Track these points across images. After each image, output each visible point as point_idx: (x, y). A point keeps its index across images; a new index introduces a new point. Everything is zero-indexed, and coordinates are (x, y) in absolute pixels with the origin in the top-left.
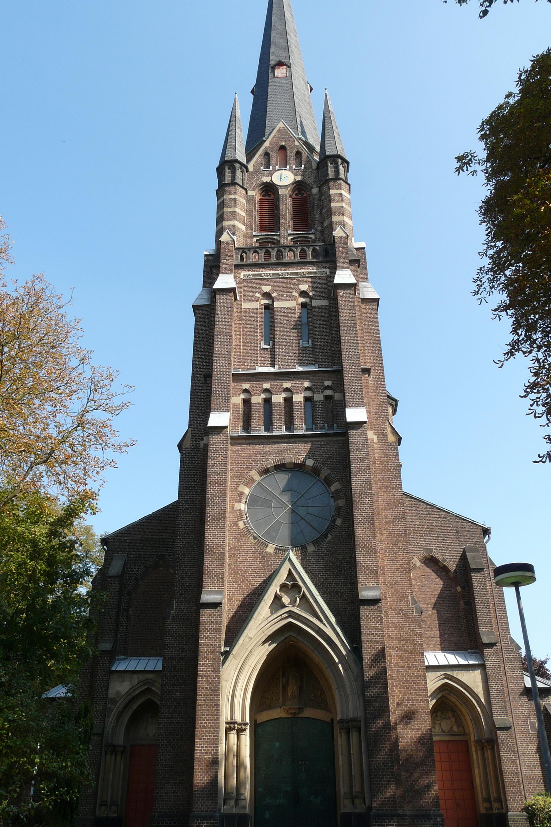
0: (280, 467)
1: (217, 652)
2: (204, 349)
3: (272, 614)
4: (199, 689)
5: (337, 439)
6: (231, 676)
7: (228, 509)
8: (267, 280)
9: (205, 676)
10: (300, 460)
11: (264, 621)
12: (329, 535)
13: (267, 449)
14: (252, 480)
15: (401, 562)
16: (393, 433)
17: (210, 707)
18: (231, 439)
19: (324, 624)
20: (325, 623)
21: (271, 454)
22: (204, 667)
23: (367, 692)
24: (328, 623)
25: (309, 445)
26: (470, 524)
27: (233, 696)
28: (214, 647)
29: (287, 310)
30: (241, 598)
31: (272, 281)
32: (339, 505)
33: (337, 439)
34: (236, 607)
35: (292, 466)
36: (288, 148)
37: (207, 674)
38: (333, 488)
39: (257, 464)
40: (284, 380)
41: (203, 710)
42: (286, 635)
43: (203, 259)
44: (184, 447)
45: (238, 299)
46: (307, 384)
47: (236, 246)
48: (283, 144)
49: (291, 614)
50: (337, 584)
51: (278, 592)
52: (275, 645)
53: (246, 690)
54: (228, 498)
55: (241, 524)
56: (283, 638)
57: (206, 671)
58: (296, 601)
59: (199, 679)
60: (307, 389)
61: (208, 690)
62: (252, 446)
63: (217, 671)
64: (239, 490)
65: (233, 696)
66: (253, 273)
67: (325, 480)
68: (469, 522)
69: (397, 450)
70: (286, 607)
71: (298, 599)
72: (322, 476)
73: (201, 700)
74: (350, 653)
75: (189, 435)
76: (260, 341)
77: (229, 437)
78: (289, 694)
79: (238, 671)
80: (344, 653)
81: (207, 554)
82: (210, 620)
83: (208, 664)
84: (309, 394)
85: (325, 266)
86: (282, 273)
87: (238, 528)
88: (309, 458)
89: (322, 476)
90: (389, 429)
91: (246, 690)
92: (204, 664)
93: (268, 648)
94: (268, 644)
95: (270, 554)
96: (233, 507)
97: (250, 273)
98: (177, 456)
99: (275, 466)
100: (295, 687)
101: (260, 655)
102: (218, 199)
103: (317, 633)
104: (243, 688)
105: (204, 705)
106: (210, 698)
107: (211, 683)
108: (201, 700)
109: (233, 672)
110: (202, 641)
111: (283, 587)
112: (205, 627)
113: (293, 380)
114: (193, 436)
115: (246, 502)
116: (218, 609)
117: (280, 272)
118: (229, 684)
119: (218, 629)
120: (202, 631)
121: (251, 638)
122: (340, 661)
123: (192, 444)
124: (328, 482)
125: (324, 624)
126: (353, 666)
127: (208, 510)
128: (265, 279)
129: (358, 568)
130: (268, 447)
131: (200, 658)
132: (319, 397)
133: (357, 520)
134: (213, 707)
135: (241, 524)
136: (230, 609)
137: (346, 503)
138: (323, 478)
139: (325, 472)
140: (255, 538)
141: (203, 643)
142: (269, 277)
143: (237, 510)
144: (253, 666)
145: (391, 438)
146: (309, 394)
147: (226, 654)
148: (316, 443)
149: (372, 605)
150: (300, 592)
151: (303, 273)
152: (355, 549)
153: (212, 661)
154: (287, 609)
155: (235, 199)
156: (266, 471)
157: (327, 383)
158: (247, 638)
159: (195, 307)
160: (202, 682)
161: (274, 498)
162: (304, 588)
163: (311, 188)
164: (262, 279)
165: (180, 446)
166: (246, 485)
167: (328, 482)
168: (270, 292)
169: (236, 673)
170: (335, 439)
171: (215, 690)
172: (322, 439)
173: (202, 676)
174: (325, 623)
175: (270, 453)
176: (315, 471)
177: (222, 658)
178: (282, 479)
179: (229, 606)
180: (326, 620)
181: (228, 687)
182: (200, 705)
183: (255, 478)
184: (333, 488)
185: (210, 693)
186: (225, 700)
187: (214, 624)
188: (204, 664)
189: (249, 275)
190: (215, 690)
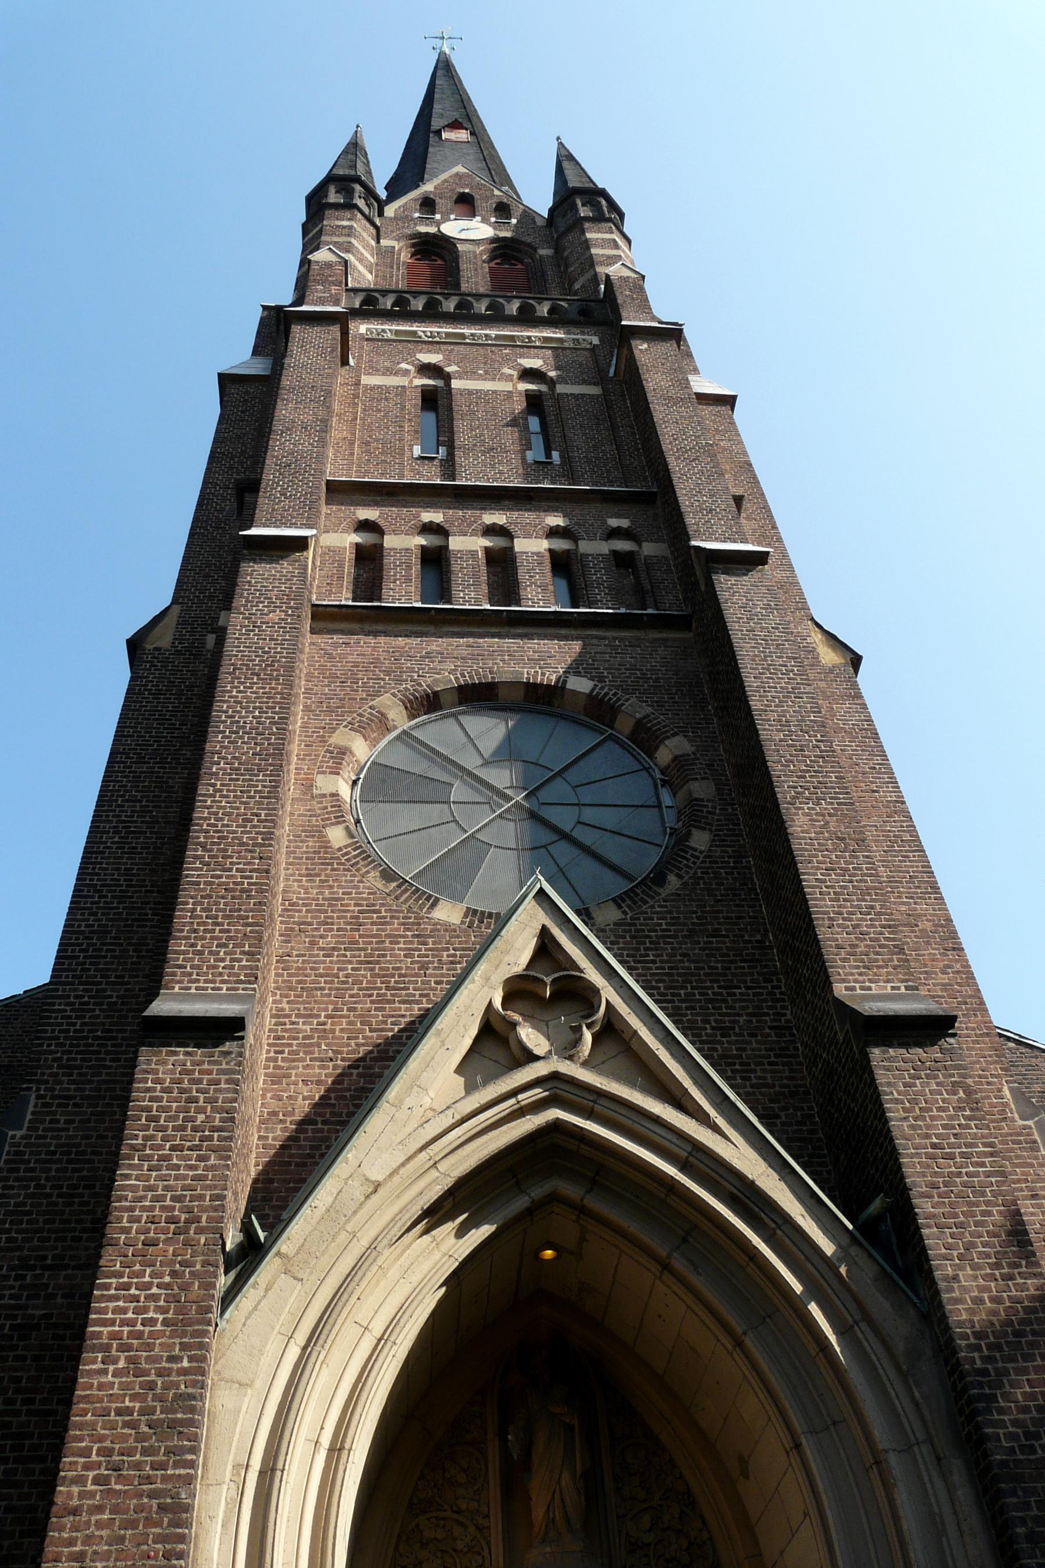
0: (479, 696)
1: (200, 1231)
2: (243, 453)
3: (470, 1088)
4: (83, 1416)
5: (664, 635)
6: (266, 1362)
7: (291, 789)
8: (432, 344)
9: (122, 1348)
10: (550, 677)
11: (432, 1119)
12: (672, 878)
13: (434, 648)
14: (383, 724)
15: (944, 979)
16: (833, 648)
17: (132, 1524)
18: (314, 617)
19: (716, 1129)
20: (721, 1122)
21: (449, 660)
22: (123, 1305)
23: (994, 1424)
24: (731, 1123)
25: (576, 646)
26: (1012, 1045)
27: (270, 1472)
28: (189, 1210)
29: (486, 395)
30: (327, 1074)
31: (443, 347)
32: (696, 795)
33: (664, 635)
34: (302, 1107)
35: (520, 694)
36: (477, 197)
37: (139, 1335)
38: (664, 755)
39: (399, 681)
40: (484, 509)
41: (88, 1540)
42: (538, 1192)
43: (258, 314)
44: (148, 647)
45: (352, 362)
46: (556, 520)
47: (350, 285)
48: (467, 191)
49: (559, 1089)
50: (725, 1032)
51: (498, 1004)
52: (484, 1231)
53: (337, 1450)
54: (295, 748)
55: (336, 836)
56: (521, 1203)
57: (131, 1323)
58: (578, 1041)
59: (91, 1363)
60: (553, 533)
61: (133, 1425)
62: (382, 639)
63: (192, 1327)
64: (332, 741)
65: (270, 1472)
66: (394, 327)
67: (633, 736)
68: (1009, 1039)
69: (855, 685)
70: (537, 1058)
71: (588, 1036)
72: (624, 725)
73: (80, 1480)
74: (854, 1250)
75: (172, 620)
76: (411, 446)
77: (307, 613)
78: (538, 1514)
79: (301, 1338)
80: (828, 1248)
81: (194, 871)
82: (182, 1091)
83: (148, 1286)
84: (561, 545)
85: (586, 331)
86: (472, 335)
87: (326, 845)
88: (578, 674)
89: (624, 725)
90: (817, 637)
91: (337, 1450)
92: (127, 1287)
93: (450, 1247)
94: (450, 1227)
95: (447, 927)
96: (308, 786)
97: (386, 327)
98: (116, 676)
99: (460, 687)
100: (566, 1478)
101: (415, 1278)
102: (304, 237)
103: (684, 1167)
104: (326, 1441)
105: (99, 1509)
106: (138, 1466)
107: (151, 1386)
108: (80, 1480)
109: (274, 1346)
110: (132, 1179)
111: (518, 990)
112: (156, 1119)
113: (509, 509)
114: (182, 622)
115: (355, 783)
116: (227, 1046)
117: (467, 331)
118: (249, 1402)
119: (214, 1129)
120: (136, 1135)
121: (377, 1187)
122: (814, 1290)
123: (179, 638)
124: (644, 738)
125: (716, 1129)
126: (880, 1305)
127: (216, 742)
128: (425, 342)
129: (823, 933)
130: (436, 644)
131: (110, 1260)
132: (593, 547)
133: (785, 789)
134: (149, 1522)
135: (336, 836)
136: (274, 1113)
137: (717, 790)
138: (627, 731)
139: (635, 708)
140: (388, 875)
141: (134, 1189)
142: (437, 339)
143: (324, 796)
144: (377, 1328)
145: (828, 657)
146: (561, 545)
147: (249, 1255)
148: (595, 641)
149: (920, 1045)
150: (593, 1009)
151: (529, 337)
152: (797, 874)
153: (174, 1274)
154: (540, 1069)
155: (351, 227)
156: (428, 703)
157: (614, 522)
158: (355, 1183)
159: (224, 380)
160: (102, 1379)
161: (456, 777)
162: (608, 993)
163: (535, 249)
164: (418, 342)
165: (135, 645)
166: (361, 729)
167: (644, 738)
168: (441, 364)
169: (293, 1353)
170: (655, 635)
171: (175, 1424)
172: (615, 634)
173: (107, 1348)
174: (721, 1122)
175: (443, 656)
176: (598, 712)
177: (223, 1281)
178: (489, 730)
179: (269, 1093)
180: (722, 1113)
181: (244, 1423)
182: (75, 1512)
183: (391, 715)
184: (664, 755)
185: (140, 1438)
186: (225, 1493)
187: (201, 1110)
188: (127, 1287)
189: (383, 331)
190: (173, 1424)
